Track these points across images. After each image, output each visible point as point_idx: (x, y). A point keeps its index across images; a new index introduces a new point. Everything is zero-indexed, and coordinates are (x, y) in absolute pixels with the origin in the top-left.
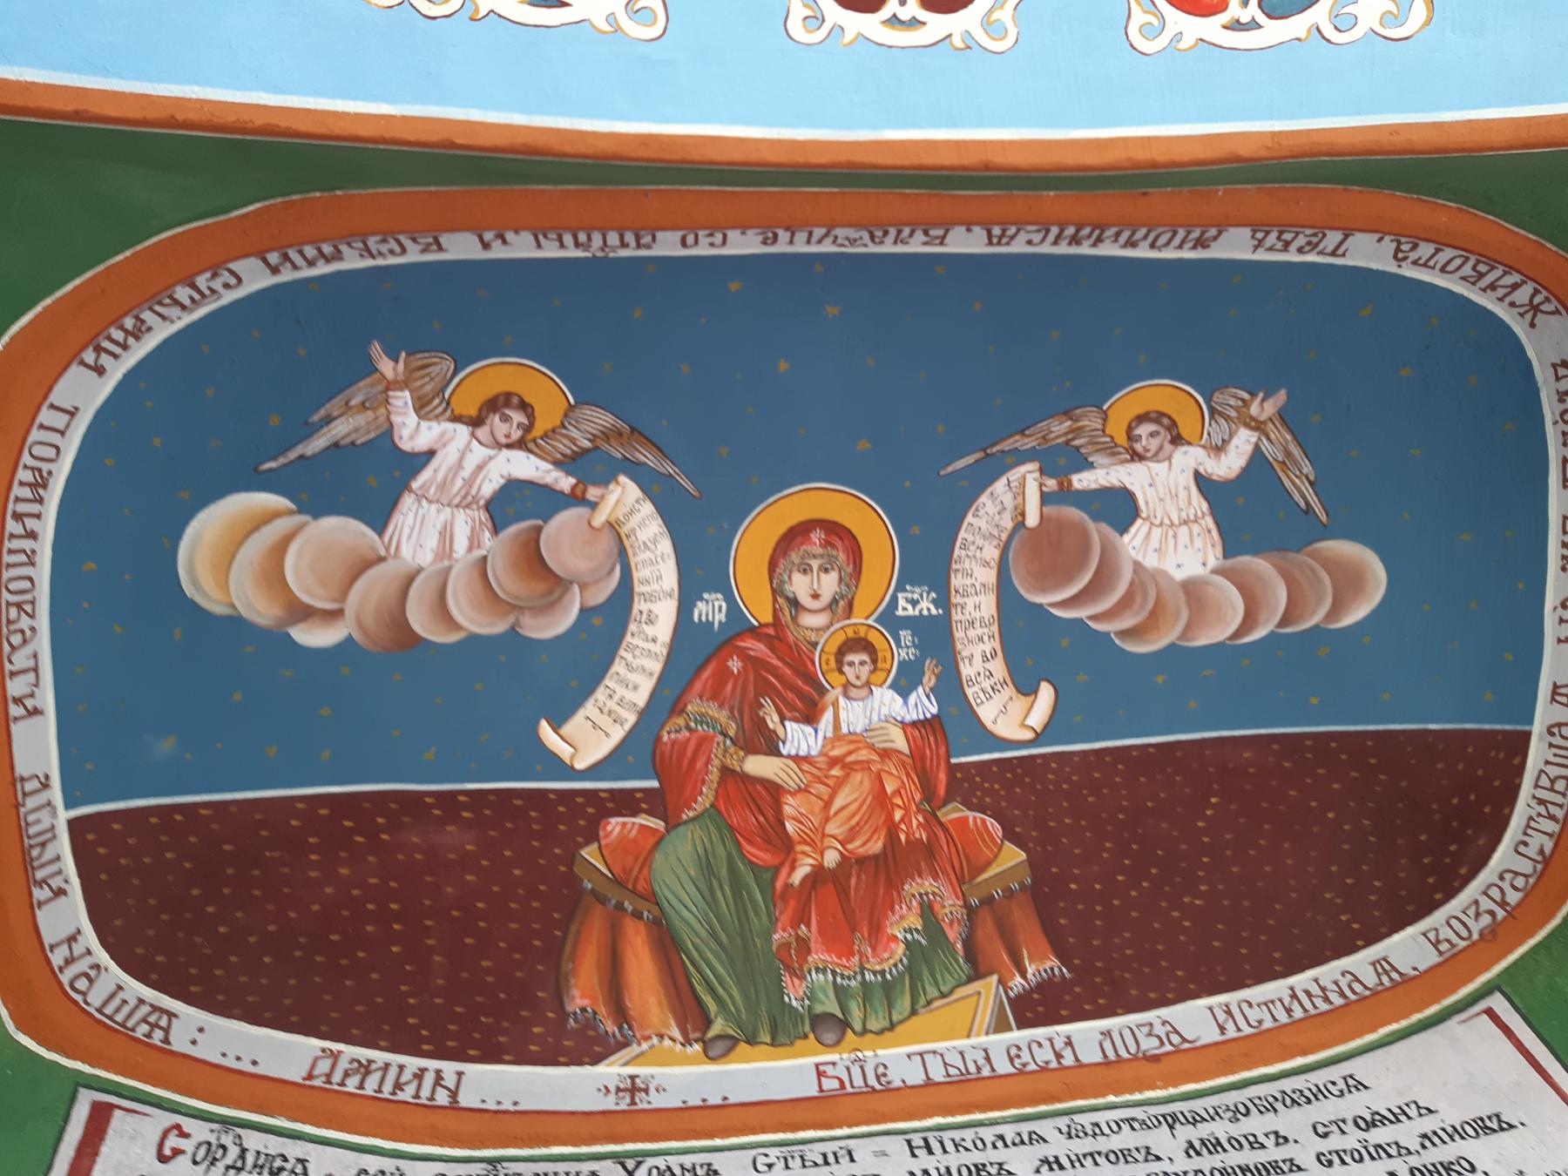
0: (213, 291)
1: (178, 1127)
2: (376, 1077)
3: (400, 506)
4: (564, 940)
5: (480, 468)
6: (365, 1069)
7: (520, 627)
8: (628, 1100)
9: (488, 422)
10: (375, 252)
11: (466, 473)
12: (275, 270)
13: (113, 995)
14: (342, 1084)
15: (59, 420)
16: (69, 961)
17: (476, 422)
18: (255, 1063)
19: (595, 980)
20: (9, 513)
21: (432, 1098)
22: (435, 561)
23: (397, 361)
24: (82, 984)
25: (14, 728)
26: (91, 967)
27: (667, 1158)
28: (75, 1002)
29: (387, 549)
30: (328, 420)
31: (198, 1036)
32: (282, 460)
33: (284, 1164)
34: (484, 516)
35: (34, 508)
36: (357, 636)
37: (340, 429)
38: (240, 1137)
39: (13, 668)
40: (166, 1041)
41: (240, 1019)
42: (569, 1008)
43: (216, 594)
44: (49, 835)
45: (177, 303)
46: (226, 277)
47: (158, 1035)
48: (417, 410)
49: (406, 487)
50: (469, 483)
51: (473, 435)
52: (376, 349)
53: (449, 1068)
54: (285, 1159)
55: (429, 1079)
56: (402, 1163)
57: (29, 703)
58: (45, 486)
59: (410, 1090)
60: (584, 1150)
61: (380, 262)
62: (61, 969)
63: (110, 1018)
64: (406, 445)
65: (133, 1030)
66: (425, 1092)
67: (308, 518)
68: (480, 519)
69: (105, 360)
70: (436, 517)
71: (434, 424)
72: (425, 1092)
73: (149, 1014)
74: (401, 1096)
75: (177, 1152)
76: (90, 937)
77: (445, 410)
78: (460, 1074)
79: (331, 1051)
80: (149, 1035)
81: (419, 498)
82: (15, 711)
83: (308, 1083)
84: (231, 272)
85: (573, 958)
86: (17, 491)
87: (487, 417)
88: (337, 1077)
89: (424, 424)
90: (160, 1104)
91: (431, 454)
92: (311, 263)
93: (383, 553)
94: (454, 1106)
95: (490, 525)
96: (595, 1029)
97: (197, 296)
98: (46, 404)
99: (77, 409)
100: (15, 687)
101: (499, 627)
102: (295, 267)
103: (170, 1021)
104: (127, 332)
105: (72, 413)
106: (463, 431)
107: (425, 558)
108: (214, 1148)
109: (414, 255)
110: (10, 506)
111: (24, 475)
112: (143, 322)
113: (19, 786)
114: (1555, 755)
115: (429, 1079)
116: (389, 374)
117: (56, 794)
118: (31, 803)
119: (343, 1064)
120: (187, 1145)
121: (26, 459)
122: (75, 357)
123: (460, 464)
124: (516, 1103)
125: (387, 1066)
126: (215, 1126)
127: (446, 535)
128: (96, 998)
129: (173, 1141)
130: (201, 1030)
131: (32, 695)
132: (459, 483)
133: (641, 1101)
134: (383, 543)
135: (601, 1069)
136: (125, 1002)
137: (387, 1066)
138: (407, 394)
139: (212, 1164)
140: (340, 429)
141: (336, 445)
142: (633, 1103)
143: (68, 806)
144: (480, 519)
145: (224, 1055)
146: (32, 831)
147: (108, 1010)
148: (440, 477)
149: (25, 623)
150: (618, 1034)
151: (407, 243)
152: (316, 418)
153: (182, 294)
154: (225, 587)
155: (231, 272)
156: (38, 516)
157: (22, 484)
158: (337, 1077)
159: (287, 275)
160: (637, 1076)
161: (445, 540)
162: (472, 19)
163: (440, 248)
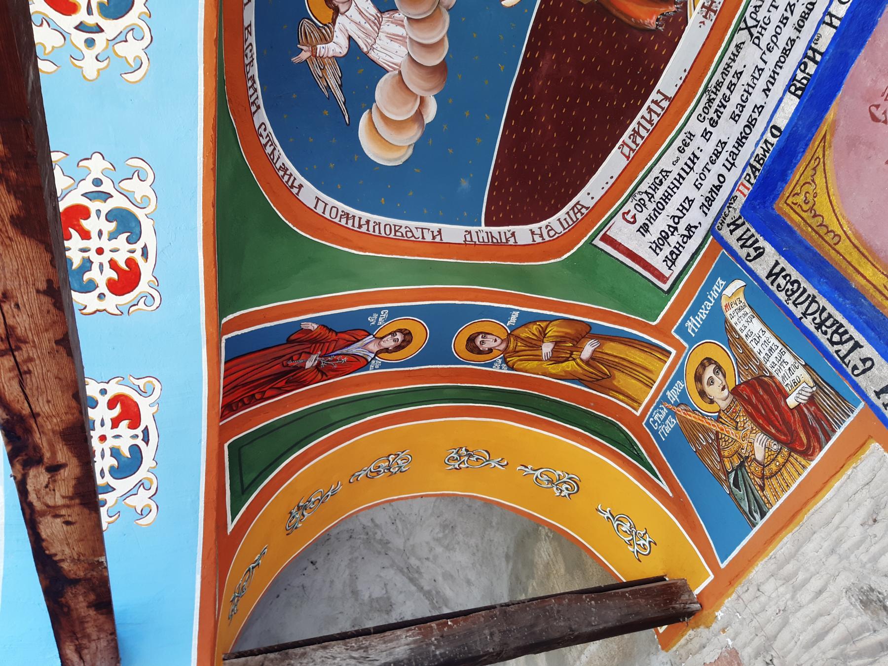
0: (268, 135)
1: (624, 214)
2: (641, 130)
3: (375, 59)
4: (617, 18)
5: (361, 13)
6: (636, 133)
7: (448, 6)
8: (712, 14)
9: (337, 4)
10: (251, 59)
11: (363, 21)
12: (258, 107)
13: (561, 223)
14: (637, 145)
15: (321, 205)
16: (541, 236)
17: (337, 11)
18: (612, 177)
19: (645, 9)
20: (358, 230)
21: (663, 109)
22: (405, 46)
23: (302, 50)
24: (552, 233)
25: (444, 241)
26: (546, 228)
27: (750, 5)
28: (558, 237)
29: (395, 69)
30: (328, 88)
31: (591, 196)
32: (345, 113)
33: (659, 179)
34: (386, 15)
35: (357, 220)
36: (436, 92)
37: (333, 83)
38: (639, 192)
39: (421, 237)
40: (587, 208)
41: (590, 177)
42: (654, 27)
43: (403, 152)
44: (489, 234)
45: (273, 152)
46: (262, 130)
47: (584, 211)
48: (327, 42)
49: (366, 55)
50: (368, 20)
51: (343, 14)
52: (295, 60)
53: (654, 96)
54: (658, 178)
55: (654, 107)
56: (684, 131)
57: (436, 233)
58: (348, 214)
59: (654, 117)
60: (724, 45)
61: (255, 56)
62: (543, 239)
63: (569, 226)
64: (345, 51)
65: (577, 219)
66: (659, 110)
67: (374, 105)
68: (387, 18)
69: (296, 184)
70: (383, 41)
71: (335, 34)
72: (659, 110)
73: (574, 212)
74: (655, 122)
75: (634, 217)
76: (535, 227)
77: (328, 27)
78: (659, 92)
79: (621, 145)
80: (582, 214)
81: (372, 48)
82: (438, 239)
83: (630, 160)
84: (260, 127)
85: (629, 17)
86: (350, 225)
87: (334, 5)
88: (634, 146)
89: (335, 39)
90: (612, 217)
91: (350, 38)
92: (256, 90)
93: (397, 72)
94: (671, 100)
95: (391, 13)
96: (669, 17)
97: (270, 143)
98: (314, 210)
99: (316, 197)
100: (428, 238)
101: (447, 17)
102: (257, 98)
103: (580, 205)
104: (285, 174)
105: (318, 199)
106: (340, 19)
107: (403, 51)
108: (639, 203)
109: (252, 39)
110: (356, 229)
111: (343, 222)
112: (281, 167)
113: (467, 242)
114: (565, 219)
115: (654, 107)
116: (308, 54)
117: (473, 229)
118: (475, 239)
119: (629, 142)
120: (633, 212)
121: (337, 220)
122: (295, 197)
123: (358, 24)
124: (685, 71)
125: (639, 123)
126: (631, 200)
127: (393, 38)
128: (559, 229)
129: (629, 217)
130: (589, 194)
131: (433, 232)
132: (367, 26)
133: (716, 7)
134: (392, 71)
135: (690, 22)
136: (565, 219)
137: (639, 123)
138: (318, 46)
139: (645, 206)
140: (333, 83)
141: (340, 86)
142: (715, 12)
143: (480, 225)
144: (387, 18)
145: (603, 188)
146: (486, 240)
147: (566, 226)
148: (363, 36)
149: (403, 230)
150: (678, 6)
151: (247, 43)
152: (326, 93)
153: (269, 150)
154: (399, 148)
155: (260, 127)
156: (360, 218)
157: (347, 223)
158: (634, 146)
159: (260, 102)
160: (704, 3)
161: (397, 39)
162: (150, 17)
163: (250, 25)
